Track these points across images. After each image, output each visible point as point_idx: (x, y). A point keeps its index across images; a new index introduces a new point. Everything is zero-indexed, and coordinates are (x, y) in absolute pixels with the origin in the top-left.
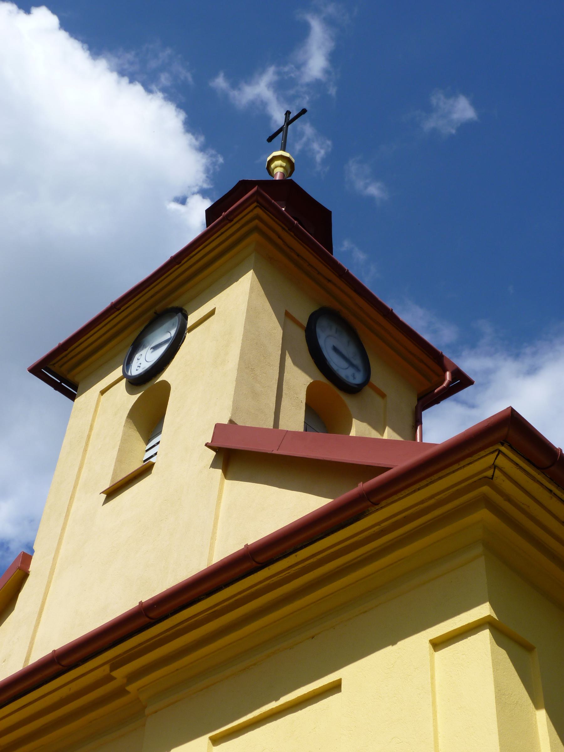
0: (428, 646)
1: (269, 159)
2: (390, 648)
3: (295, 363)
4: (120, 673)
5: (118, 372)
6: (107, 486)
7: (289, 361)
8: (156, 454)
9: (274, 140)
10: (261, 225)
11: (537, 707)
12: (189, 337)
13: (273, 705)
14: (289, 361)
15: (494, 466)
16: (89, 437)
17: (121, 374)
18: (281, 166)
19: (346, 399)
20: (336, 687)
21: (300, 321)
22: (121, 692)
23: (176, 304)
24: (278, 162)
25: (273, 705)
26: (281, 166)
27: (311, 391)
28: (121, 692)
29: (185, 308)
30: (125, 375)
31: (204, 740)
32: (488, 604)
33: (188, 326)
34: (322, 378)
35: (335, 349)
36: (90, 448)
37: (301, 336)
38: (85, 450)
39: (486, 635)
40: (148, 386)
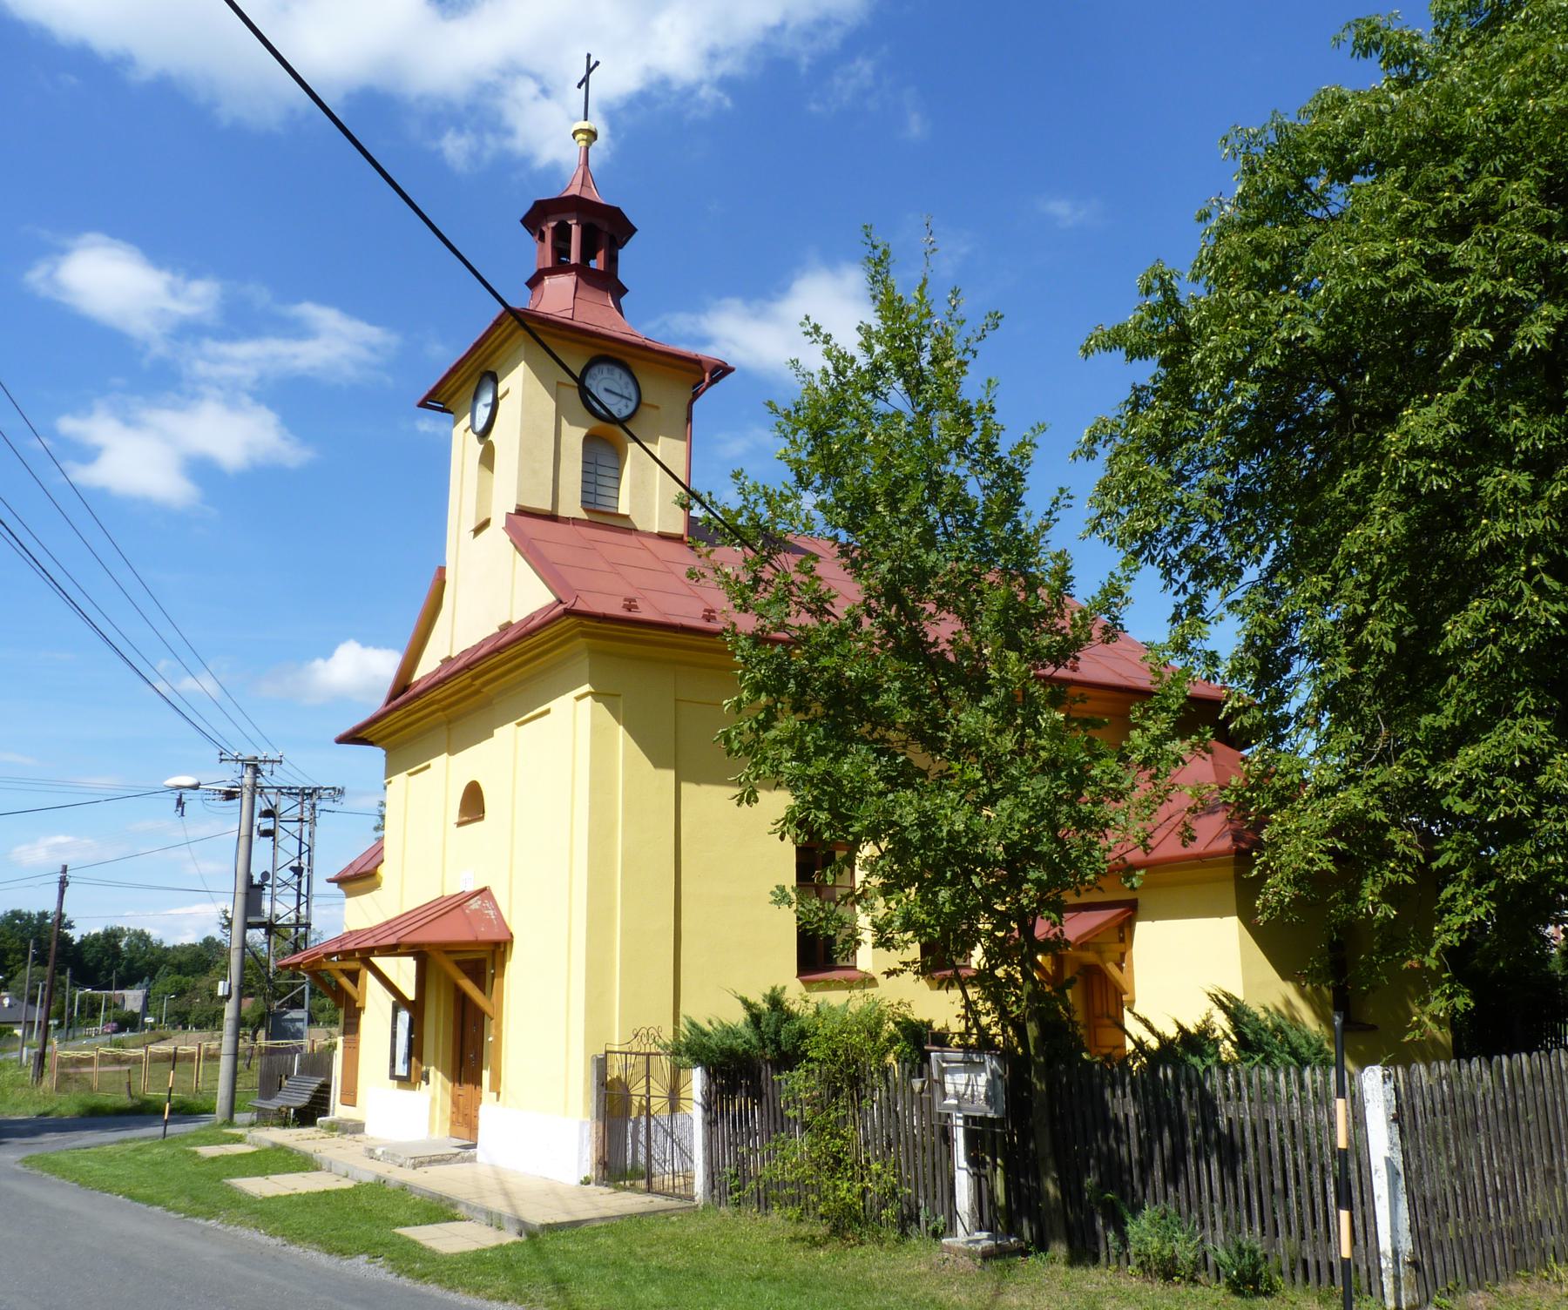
4: (478, 683)
7: (564, 422)
14: (564, 422)
20: (547, 712)
22: (478, 692)
23: (491, 369)
24: (580, 136)
27: (588, 440)
28: (478, 692)
34: (596, 423)
35: (607, 390)
39: (590, 698)
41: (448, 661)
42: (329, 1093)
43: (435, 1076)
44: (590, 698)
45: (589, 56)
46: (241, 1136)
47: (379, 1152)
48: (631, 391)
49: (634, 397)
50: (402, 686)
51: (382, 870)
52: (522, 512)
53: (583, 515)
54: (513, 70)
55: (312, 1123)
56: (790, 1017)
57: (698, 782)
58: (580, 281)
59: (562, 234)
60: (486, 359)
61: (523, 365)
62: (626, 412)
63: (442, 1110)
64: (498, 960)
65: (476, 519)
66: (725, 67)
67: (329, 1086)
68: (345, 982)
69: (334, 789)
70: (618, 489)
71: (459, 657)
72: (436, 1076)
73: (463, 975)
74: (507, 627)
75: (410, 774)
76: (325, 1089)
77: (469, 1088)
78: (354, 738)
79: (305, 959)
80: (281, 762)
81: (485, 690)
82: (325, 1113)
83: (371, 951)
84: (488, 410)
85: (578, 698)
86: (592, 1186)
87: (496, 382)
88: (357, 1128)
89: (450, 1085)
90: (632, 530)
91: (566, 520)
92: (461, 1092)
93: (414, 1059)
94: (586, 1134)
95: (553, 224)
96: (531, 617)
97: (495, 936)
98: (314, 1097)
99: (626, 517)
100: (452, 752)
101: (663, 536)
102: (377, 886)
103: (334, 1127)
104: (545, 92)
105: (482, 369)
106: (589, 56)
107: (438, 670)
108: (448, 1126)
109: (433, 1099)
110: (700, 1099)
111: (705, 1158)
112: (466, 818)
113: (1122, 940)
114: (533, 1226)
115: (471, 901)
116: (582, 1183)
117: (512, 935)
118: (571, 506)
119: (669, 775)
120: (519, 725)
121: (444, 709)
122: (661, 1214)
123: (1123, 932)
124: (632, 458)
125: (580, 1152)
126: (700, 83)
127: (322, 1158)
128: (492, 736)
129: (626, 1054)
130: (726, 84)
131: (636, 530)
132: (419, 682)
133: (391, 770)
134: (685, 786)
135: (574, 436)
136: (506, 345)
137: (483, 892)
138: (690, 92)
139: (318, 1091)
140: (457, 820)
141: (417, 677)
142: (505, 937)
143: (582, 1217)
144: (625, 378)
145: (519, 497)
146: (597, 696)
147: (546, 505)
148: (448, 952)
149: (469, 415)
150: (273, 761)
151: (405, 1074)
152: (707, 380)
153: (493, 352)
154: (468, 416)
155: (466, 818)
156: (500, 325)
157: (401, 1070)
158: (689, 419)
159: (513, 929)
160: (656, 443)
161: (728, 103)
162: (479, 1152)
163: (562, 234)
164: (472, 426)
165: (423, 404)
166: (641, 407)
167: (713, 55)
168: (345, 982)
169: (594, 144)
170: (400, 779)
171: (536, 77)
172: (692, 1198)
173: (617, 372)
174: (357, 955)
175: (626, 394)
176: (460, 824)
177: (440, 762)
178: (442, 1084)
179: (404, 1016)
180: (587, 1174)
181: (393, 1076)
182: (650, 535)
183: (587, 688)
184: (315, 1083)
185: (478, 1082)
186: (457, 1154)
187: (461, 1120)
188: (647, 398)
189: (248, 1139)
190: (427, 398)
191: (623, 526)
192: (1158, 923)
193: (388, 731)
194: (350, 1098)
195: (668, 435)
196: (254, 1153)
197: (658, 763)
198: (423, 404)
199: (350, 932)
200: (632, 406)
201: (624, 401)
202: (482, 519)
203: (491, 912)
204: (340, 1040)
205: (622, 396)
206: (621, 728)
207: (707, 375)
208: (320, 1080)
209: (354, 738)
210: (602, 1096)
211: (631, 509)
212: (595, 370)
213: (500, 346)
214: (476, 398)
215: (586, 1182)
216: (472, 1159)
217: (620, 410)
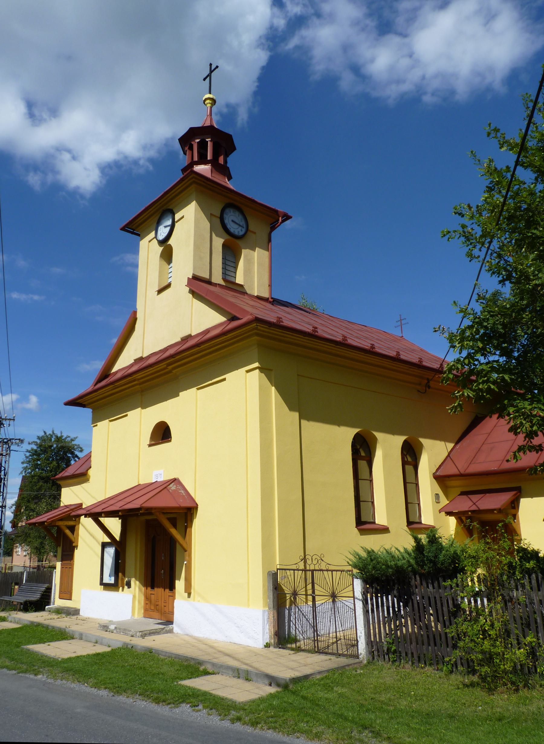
0: (245, 372)
1: (204, 99)
2: (236, 371)
3: (217, 235)
4: (170, 367)
5: (152, 234)
6: (157, 290)
7: (214, 235)
8: (183, 217)
9: (206, 80)
10: (195, 176)
11: (272, 386)
12: (177, 225)
13: (210, 382)
14: (214, 235)
15: (257, 325)
16: (148, 262)
17: (154, 236)
18: (209, 103)
19: (238, 242)
20: (224, 380)
21: (217, 215)
22: (170, 372)
23: (170, 208)
24: (208, 101)
25: (210, 382)
26: (209, 103)
27: (224, 246)
28: (170, 372)
29: (175, 210)
30: (156, 237)
31: (195, 389)
32: (257, 363)
33: (176, 220)
34: (228, 237)
35: (233, 221)
36: (149, 268)
37: (218, 221)
38: (147, 268)
39: (258, 370)
40: (165, 244)
41: (140, 360)
42: (51, 592)
43: (135, 584)
44: (258, 370)
45: (211, 65)
46: (4, 617)
47: (112, 627)
48: (243, 223)
49: (245, 226)
50: (105, 374)
51: (91, 472)
52: (195, 278)
53: (222, 283)
54: (60, 149)
55: (43, 609)
56: (441, 548)
57: (308, 420)
58: (213, 169)
59: (203, 146)
60: (169, 201)
61: (195, 201)
62: (241, 233)
63: (139, 602)
64: (189, 518)
65: (159, 285)
66: (152, 153)
67: (51, 589)
68: (68, 532)
69: (19, 439)
70: (235, 273)
71: (149, 357)
72: (135, 584)
73: (172, 526)
74: (186, 339)
75: (110, 421)
76: (48, 591)
77: (159, 591)
78: (74, 403)
79: (48, 519)
80: (14, 420)
81: (174, 371)
82: (48, 603)
83: (100, 514)
84: (168, 229)
85: (248, 371)
86: (272, 648)
87: (174, 215)
88: (76, 612)
89: (143, 589)
90: (244, 293)
91: (215, 285)
92: (153, 592)
93: (120, 574)
94: (266, 618)
95: (198, 140)
96: (207, 331)
97: (188, 504)
98: (42, 595)
99: (241, 286)
100: (144, 407)
101: (259, 298)
102: (87, 480)
103: (59, 611)
104: (74, 158)
105: (165, 208)
106: (211, 65)
107: (132, 365)
108: (143, 611)
109: (134, 597)
110: (361, 597)
111: (365, 632)
112: (153, 442)
113: (514, 508)
114: (285, 680)
115: (171, 486)
116: (265, 647)
117: (197, 504)
118: (217, 278)
119: (296, 415)
120: (198, 389)
121: (140, 384)
122: (347, 668)
123: (514, 505)
124: (244, 257)
125: (264, 629)
126: (140, 159)
127: (73, 631)
128: (178, 396)
129: (294, 570)
130: (151, 160)
131: (247, 293)
132: (117, 372)
133: (96, 420)
134: (302, 421)
135: (218, 242)
136: (183, 193)
137: (175, 481)
138: (136, 162)
139: (45, 592)
140: (148, 443)
141: (114, 370)
142: (194, 505)
143: (308, 673)
144: (241, 217)
145: (194, 270)
146: (261, 369)
147: (206, 276)
148: (163, 513)
149: (154, 232)
150: (10, 419)
151: (112, 581)
152: (280, 221)
153: (172, 199)
154: (154, 232)
155: (153, 442)
156: (183, 181)
157: (109, 579)
158: (270, 240)
159: (197, 501)
160: (255, 251)
161: (151, 168)
162: (175, 627)
163: (203, 146)
164: (156, 237)
165: (123, 229)
166: (248, 232)
167: (145, 148)
168: (68, 532)
169: (214, 106)
170: (103, 425)
171: (69, 151)
172: (357, 656)
173: (237, 213)
174: (120, 513)
175: (241, 224)
176: (150, 445)
177: (135, 414)
178: (139, 588)
179: (110, 552)
180: (268, 641)
181: (102, 583)
182: (252, 297)
183: (256, 365)
184: (43, 588)
185: (172, 587)
186: (163, 629)
187: (153, 608)
188: (251, 228)
189: (10, 619)
190: (127, 226)
191: (239, 290)
192: (534, 498)
193: (101, 396)
194: (66, 593)
195: (260, 248)
196: (20, 628)
197: (291, 409)
198: (123, 229)
199: (66, 506)
200: (244, 230)
201: (240, 228)
202: (166, 284)
203: (183, 492)
204: (59, 565)
205: (240, 225)
206: (273, 388)
207: (280, 218)
208: (46, 585)
209: (74, 403)
210: (275, 595)
211: (244, 282)
212: (227, 210)
213: (177, 195)
214: (159, 223)
215: (267, 646)
216: (171, 631)
217: (238, 232)
